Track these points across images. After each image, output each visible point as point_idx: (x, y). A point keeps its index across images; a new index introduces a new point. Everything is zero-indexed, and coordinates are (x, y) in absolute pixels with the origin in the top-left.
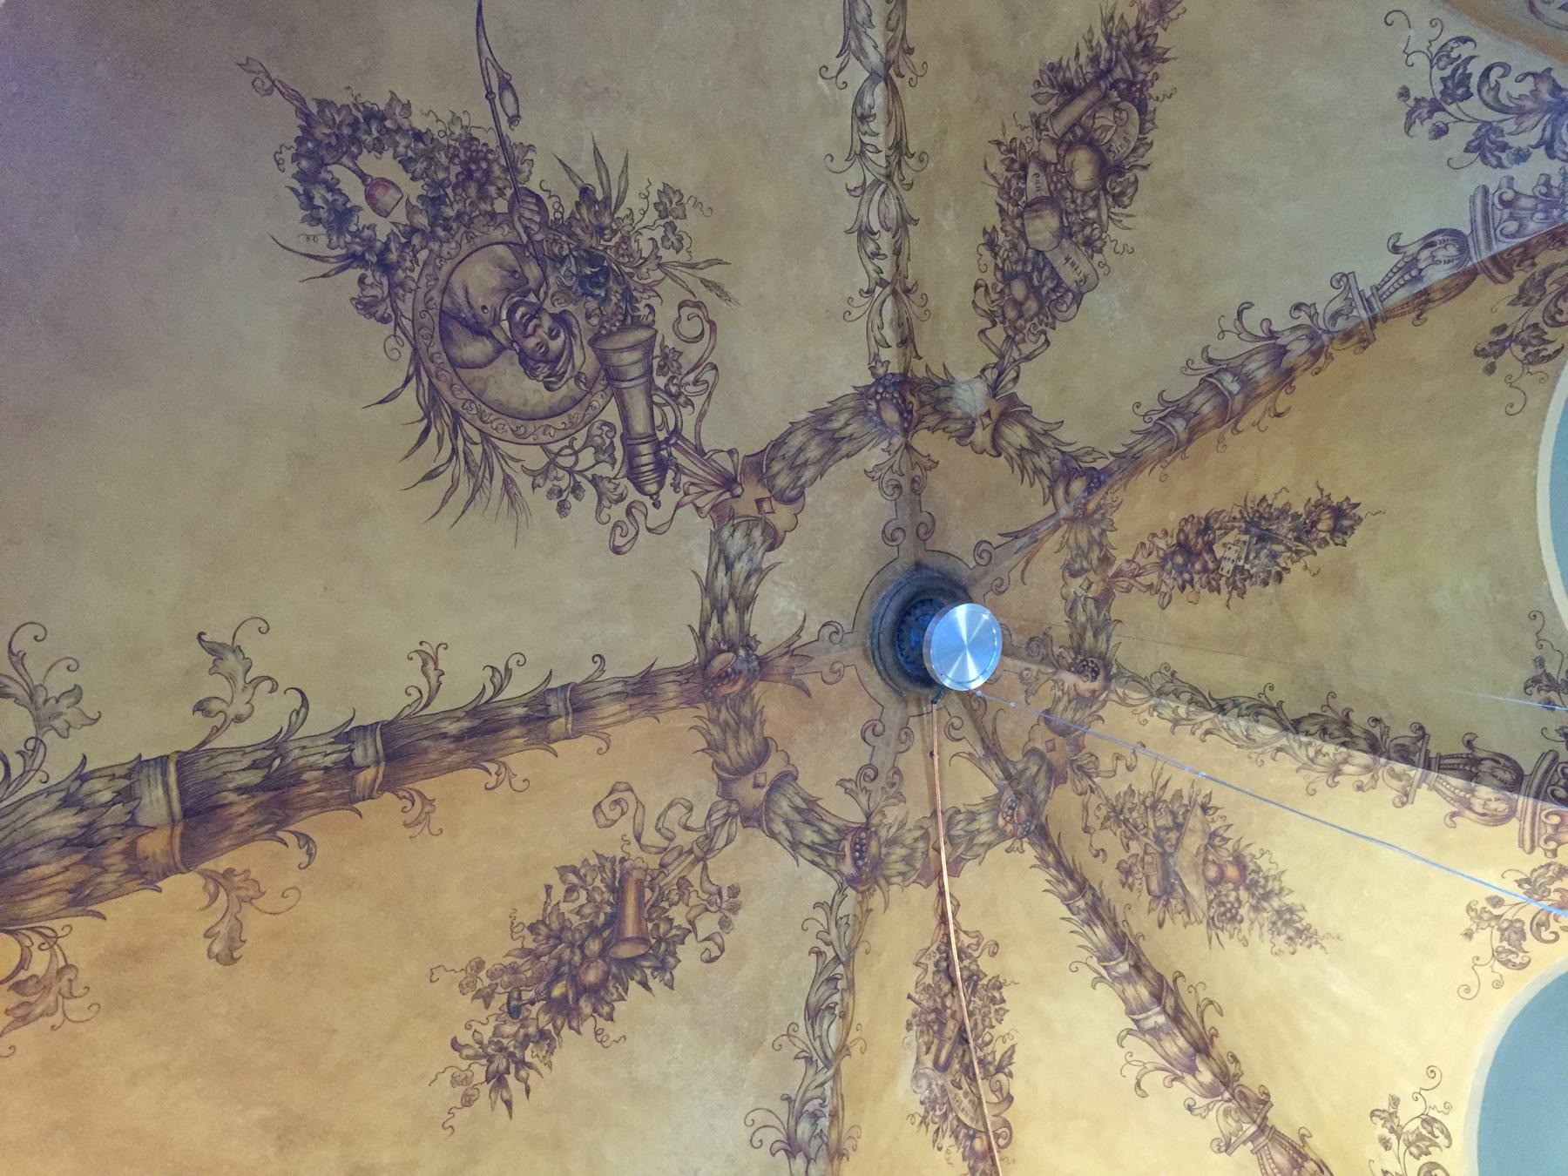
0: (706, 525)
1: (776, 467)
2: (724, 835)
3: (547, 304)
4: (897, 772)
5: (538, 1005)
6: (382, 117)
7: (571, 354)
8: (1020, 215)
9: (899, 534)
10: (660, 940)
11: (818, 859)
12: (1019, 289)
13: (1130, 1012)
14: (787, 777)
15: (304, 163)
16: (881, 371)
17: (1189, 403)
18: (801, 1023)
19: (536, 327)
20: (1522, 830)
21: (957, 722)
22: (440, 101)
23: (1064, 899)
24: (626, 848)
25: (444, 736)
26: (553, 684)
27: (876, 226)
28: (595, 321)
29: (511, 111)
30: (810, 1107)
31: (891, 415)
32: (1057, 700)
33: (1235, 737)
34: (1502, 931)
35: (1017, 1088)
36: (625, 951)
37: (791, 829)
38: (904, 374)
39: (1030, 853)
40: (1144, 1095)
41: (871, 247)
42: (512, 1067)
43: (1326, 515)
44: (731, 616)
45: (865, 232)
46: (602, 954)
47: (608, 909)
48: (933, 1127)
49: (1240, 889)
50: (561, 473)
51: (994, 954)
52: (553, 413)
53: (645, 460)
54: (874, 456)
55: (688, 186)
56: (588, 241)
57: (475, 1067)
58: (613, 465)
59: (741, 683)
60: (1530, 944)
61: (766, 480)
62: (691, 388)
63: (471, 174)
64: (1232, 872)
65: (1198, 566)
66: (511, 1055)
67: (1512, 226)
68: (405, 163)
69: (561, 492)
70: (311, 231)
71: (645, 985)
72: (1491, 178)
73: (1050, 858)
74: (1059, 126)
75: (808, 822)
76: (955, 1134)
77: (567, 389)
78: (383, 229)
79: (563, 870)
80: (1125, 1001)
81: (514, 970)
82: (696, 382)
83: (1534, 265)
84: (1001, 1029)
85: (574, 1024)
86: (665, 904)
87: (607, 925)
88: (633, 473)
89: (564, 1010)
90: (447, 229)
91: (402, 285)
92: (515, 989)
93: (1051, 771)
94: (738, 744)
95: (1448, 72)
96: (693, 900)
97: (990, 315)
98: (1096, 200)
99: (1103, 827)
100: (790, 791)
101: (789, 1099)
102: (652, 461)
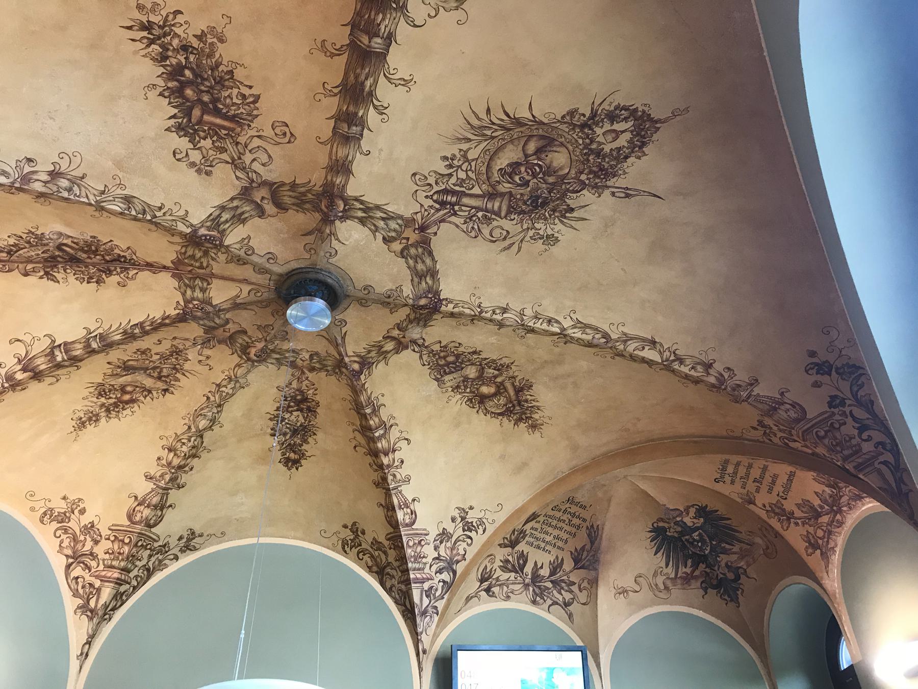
0: (407, 214)
1: (420, 250)
2: (242, 176)
3: (535, 180)
4: (244, 264)
5: (183, 61)
6: (641, 147)
7: (510, 183)
8: (481, 365)
9: (366, 292)
10: (195, 131)
11: (211, 217)
12: (451, 359)
13: (66, 344)
14: (262, 213)
15: (640, 113)
16: (444, 303)
17: (376, 416)
18: (125, 192)
19: (528, 173)
20: (122, 526)
21: (259, 294)
22: (634, 171)
23: (142, 323)
24: (255, 129)
25: (366, 79)
26: (366, 131)
27: (505, 315)
28: (518, 196)
29: (617, 194)
30: (76, 188)
31: (423, 302)
32: (250, 338)
33: (202, 409)
34: (65, 513)
35: (32, 279)
36: (196, 113)
37: (232, 208)
38: (438, 311)
39: (174, 313)
40: (11, 342)
41: (498, 311)
42: (152, 37)
43: (297, 457)
44: (360, 214)
45: (505, 310)
46: (200, 101)
47: (224, 111)
48: (24, 236)
49: (115, 400)
50: (461, 162)
51: (119, 283)
52: (489, 167)
53: (449, 198)
54: (408, 290)
55: (555, 250)
56: (551, 205)
57: (160, 18)
58: (454, 185)
59: (326, 210)
60: (55, 525)
61: (416, 245)
62: (471, 225)
63: (600, 170)
64: (127, 397)
65: (292, 404)
66: (159, 38)
67: (411, 543)
68: (619, 149)
69: (452, 160)
70: (614, 104)
71: (174, 117)
72: (431, 538)
73: (167, 321)
74: (508, 385)
75: (234, 216)
76: (15, 245)
77: (496, 176)
78: (599, 131)
79: (257, 98)
80: (73, 342)
81: (210, 55)
82: (473, 228)
83: (390, 548)
84: (71, 278)
85: (164, 76)
86: (215, 138)
87: (216, 108)
88: (446, 191)
89: (175, 73)
90: (585, 154)
91: (573, 129)
92: (199, 53)
93: (214, 328)
94: (290, 196)
95: (474, 524)
96: (211, 152)
97: (445, 347)
98: (474, 392)
99: (172, 345)
100: (253, 213)
101: (83, 178)
102: (447, 201)
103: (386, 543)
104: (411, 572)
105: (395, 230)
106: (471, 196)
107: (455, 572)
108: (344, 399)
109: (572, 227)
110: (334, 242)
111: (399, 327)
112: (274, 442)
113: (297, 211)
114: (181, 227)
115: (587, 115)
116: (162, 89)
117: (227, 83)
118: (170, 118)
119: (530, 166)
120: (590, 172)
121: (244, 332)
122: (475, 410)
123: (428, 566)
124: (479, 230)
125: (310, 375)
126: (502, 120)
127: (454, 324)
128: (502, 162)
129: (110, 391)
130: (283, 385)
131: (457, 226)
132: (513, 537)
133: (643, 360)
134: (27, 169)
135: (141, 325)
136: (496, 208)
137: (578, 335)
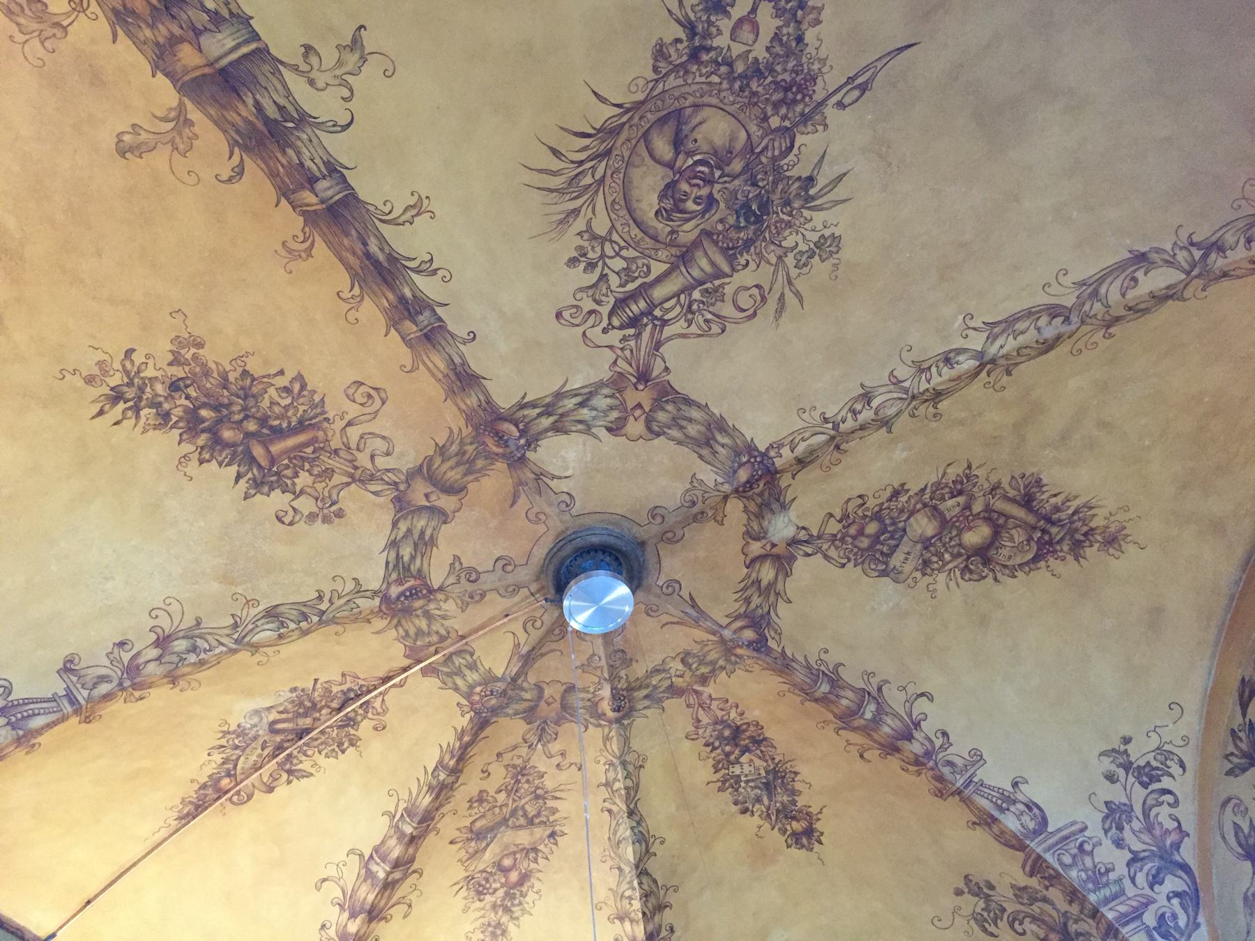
0: (606, 375)
1: (670, 407)
2: (379, 488)
3: (717, 187)
5: (187, 403)
8: (925, 505)
9: (659, 520)
10: (278, 474)
11: (391, 566)
12: (872, 528)
13: (376, 849)
14: (443, 516)
16: (772, 453)
17: (843, 688)
18: (261, 608)
21: (538, 624)
25: (365, 244)
26: (439, 310)
27: (875, 404)
28: (720, 227)
29: (847, 101)
30: (200, 642)
31: (743, 475)
32: (585, 690)
33: (615, 834)
35: (282, 791)
36: (258, 451)
38: (777, 472)
41: (858, 407)
42: (131, 403)
43: (804, 824)
44: (546, 422)
45: (867, 397)
46: (248, 435)
47: (285, 425)
48: (223, 742)
50: (598, 249)
51: (376, 729)
53: (634, 308)
54: (709, 476)
55: (847, 253)
56: (776, 197)
57: (118, 375)
58: (621, 286)
59: (500, 450)
61: (658, 404)
64: (514, 876)
65: (728, 748)
66: (140, 399)
67: (1067, 859)
68: (777, 37)
69: (584, 255)
71: (239, 477)
73: (466, 739)
74: (1000, 505)
75: (416, 545)
77: (662, 228)
78: (722, 41)
79: (299, 377)
80: (383, 842)
81: (207, 373)
82: (706, 321)
83: (1047, 888)
84: (321, 760)
85: (185, 436)
86: (307, 466)
88: (621, 303)
89: (192, 424)
90: (742, 89)
91: (687, 72)
92: (193, 380)
94: (452, 468)
95: (1154, 764)
96: (319, 486)
97: (845, 516)
98: (960, 555)
99: (507, 767)
100: (433, 523)
101: (198, 624)
102: (635, 313)
103: (1034, 882)
104: (1104, 910)
105: (611, 408)
106: (659, 280)
107: (1185, 868)
108: (781, 694)
109: (837, 203)
110: (553, 484)
111: (751, 536)
112: (752, 822)
113: (477, 480)
114: (365, 604)
115: (683, 36)
116: (196, 455)
117: (255, 390)
118: (237, 481)
119: (691, 175)
120: (776, 106)
121: (571, 688)
122: (990, 580)
123: (1127, 883)
124: (718, 316)
125: (708, 690)
126: (586, 148)
127: (818, 472)
128: (648, 201)
129: (487, 880)
130: (691, 728)
131: (684, 336)
132: (1243, 746)
133: (1160, 298)
134: (126, 657)
135: (440, 764)
136: (708, 269)
137: (1009, 344)
